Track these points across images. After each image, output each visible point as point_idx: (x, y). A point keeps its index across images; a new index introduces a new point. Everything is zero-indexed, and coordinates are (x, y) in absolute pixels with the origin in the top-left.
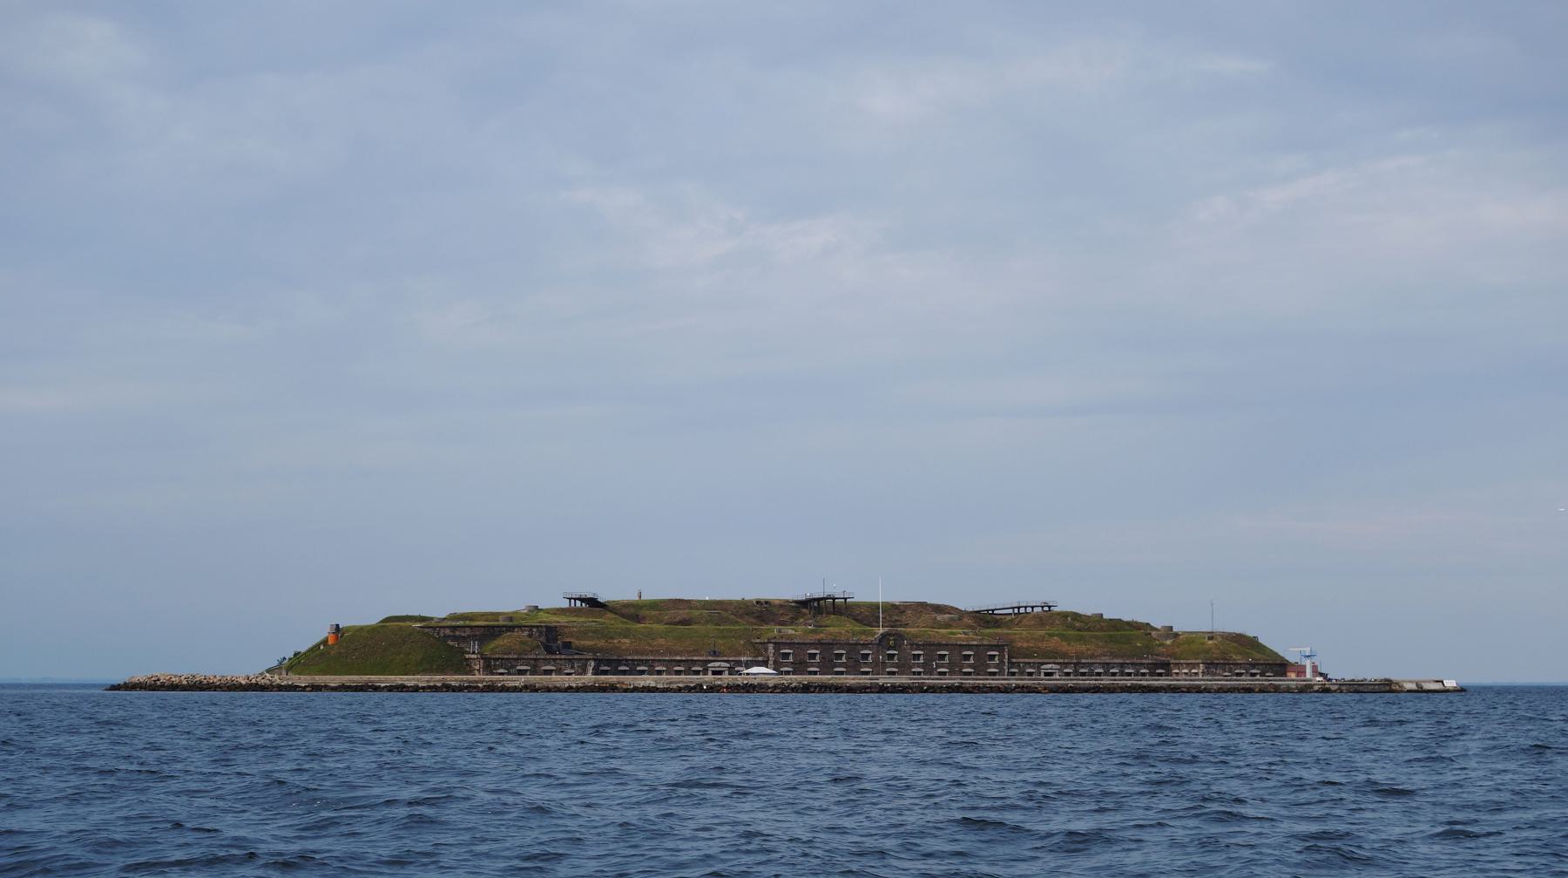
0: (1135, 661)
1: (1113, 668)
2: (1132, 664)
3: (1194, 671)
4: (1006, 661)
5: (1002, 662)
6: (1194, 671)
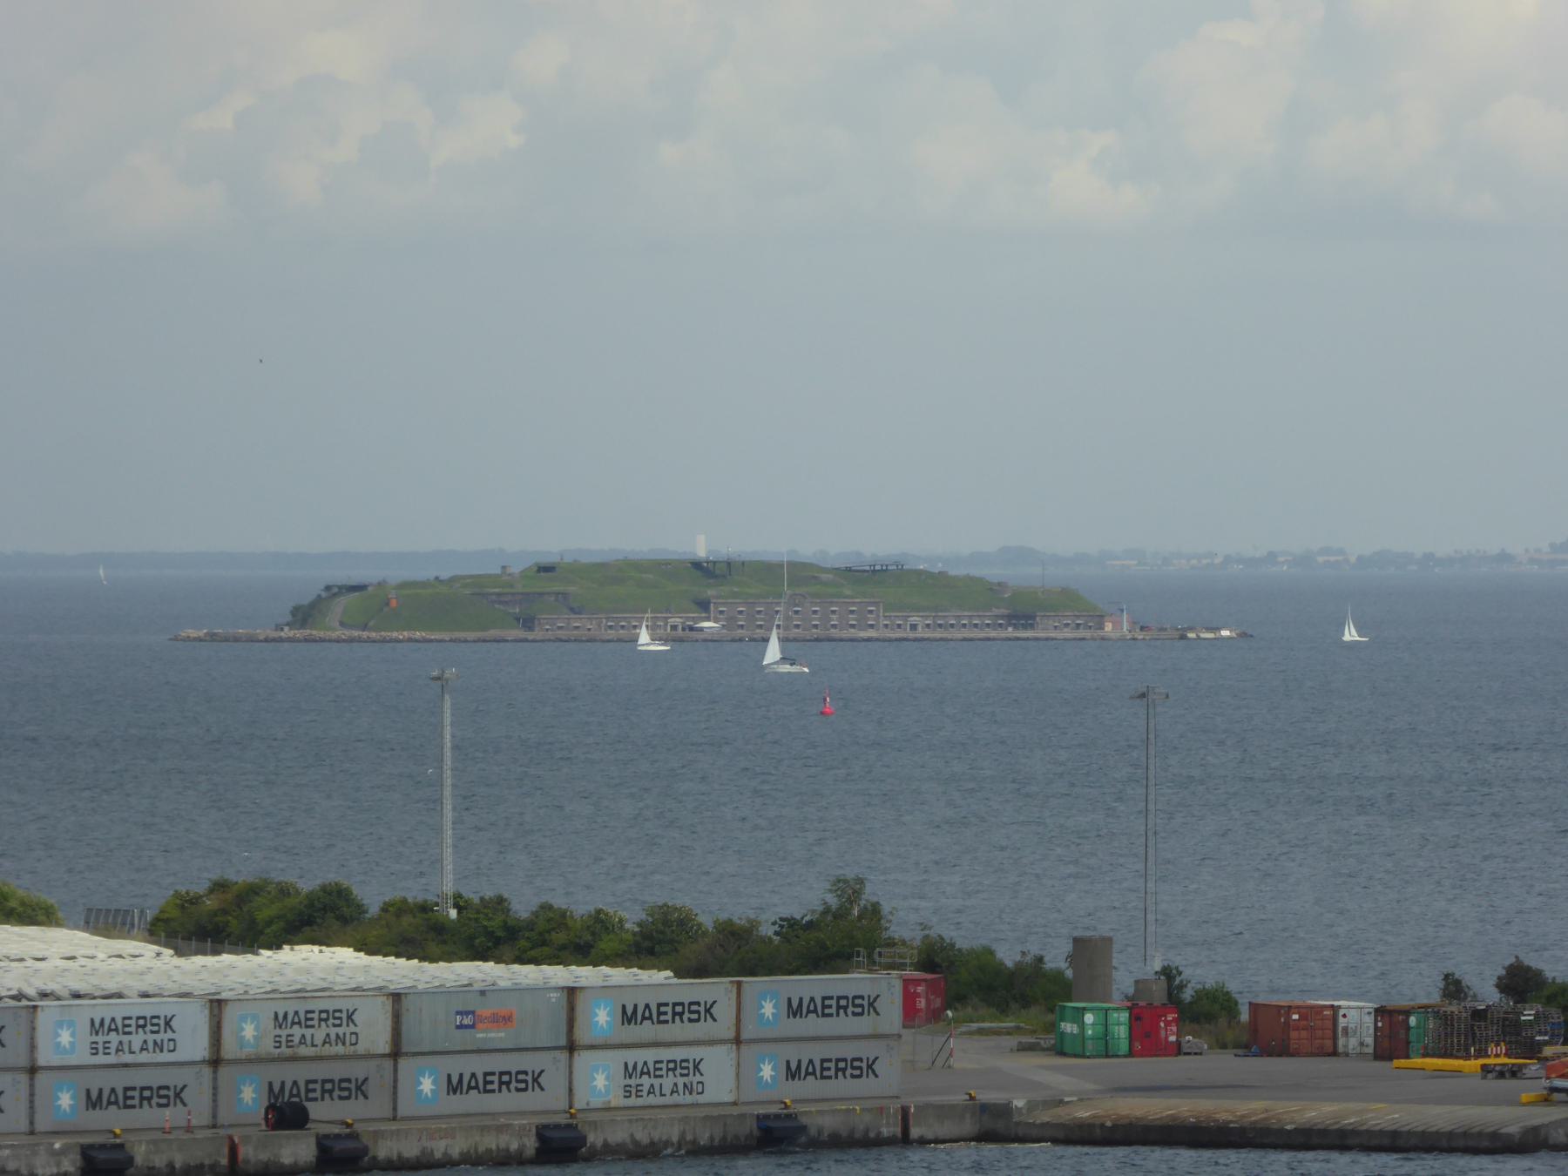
0: (981, 614)
1: (963, 620)
2: (979, 616)
3: (1029, 622)
4: (881, 614)
5: (878, 616)
6: (1029, 622)
